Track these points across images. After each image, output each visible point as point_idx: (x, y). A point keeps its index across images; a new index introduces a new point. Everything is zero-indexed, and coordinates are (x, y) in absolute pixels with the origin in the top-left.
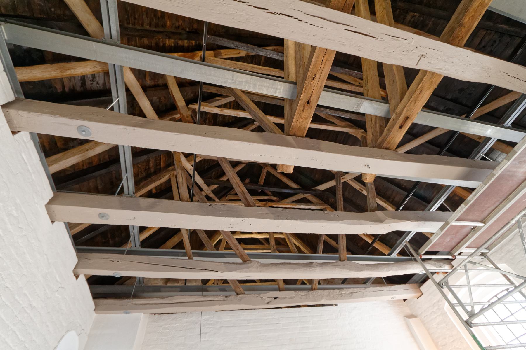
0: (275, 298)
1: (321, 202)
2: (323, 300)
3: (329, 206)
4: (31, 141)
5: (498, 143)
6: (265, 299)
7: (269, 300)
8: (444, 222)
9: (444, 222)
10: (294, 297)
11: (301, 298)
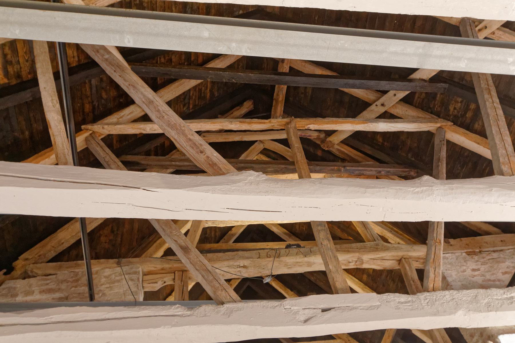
0: (324, 311)
1: (428, 116)
2: (460, 313)
3: (450, 123)
4: (35, 55)
5: (77, 77)
6: (297, 313)
7: (308, 313)
8: (408, 78)
9: (408, 78)
10: (378, 307)
11: (397, 308)
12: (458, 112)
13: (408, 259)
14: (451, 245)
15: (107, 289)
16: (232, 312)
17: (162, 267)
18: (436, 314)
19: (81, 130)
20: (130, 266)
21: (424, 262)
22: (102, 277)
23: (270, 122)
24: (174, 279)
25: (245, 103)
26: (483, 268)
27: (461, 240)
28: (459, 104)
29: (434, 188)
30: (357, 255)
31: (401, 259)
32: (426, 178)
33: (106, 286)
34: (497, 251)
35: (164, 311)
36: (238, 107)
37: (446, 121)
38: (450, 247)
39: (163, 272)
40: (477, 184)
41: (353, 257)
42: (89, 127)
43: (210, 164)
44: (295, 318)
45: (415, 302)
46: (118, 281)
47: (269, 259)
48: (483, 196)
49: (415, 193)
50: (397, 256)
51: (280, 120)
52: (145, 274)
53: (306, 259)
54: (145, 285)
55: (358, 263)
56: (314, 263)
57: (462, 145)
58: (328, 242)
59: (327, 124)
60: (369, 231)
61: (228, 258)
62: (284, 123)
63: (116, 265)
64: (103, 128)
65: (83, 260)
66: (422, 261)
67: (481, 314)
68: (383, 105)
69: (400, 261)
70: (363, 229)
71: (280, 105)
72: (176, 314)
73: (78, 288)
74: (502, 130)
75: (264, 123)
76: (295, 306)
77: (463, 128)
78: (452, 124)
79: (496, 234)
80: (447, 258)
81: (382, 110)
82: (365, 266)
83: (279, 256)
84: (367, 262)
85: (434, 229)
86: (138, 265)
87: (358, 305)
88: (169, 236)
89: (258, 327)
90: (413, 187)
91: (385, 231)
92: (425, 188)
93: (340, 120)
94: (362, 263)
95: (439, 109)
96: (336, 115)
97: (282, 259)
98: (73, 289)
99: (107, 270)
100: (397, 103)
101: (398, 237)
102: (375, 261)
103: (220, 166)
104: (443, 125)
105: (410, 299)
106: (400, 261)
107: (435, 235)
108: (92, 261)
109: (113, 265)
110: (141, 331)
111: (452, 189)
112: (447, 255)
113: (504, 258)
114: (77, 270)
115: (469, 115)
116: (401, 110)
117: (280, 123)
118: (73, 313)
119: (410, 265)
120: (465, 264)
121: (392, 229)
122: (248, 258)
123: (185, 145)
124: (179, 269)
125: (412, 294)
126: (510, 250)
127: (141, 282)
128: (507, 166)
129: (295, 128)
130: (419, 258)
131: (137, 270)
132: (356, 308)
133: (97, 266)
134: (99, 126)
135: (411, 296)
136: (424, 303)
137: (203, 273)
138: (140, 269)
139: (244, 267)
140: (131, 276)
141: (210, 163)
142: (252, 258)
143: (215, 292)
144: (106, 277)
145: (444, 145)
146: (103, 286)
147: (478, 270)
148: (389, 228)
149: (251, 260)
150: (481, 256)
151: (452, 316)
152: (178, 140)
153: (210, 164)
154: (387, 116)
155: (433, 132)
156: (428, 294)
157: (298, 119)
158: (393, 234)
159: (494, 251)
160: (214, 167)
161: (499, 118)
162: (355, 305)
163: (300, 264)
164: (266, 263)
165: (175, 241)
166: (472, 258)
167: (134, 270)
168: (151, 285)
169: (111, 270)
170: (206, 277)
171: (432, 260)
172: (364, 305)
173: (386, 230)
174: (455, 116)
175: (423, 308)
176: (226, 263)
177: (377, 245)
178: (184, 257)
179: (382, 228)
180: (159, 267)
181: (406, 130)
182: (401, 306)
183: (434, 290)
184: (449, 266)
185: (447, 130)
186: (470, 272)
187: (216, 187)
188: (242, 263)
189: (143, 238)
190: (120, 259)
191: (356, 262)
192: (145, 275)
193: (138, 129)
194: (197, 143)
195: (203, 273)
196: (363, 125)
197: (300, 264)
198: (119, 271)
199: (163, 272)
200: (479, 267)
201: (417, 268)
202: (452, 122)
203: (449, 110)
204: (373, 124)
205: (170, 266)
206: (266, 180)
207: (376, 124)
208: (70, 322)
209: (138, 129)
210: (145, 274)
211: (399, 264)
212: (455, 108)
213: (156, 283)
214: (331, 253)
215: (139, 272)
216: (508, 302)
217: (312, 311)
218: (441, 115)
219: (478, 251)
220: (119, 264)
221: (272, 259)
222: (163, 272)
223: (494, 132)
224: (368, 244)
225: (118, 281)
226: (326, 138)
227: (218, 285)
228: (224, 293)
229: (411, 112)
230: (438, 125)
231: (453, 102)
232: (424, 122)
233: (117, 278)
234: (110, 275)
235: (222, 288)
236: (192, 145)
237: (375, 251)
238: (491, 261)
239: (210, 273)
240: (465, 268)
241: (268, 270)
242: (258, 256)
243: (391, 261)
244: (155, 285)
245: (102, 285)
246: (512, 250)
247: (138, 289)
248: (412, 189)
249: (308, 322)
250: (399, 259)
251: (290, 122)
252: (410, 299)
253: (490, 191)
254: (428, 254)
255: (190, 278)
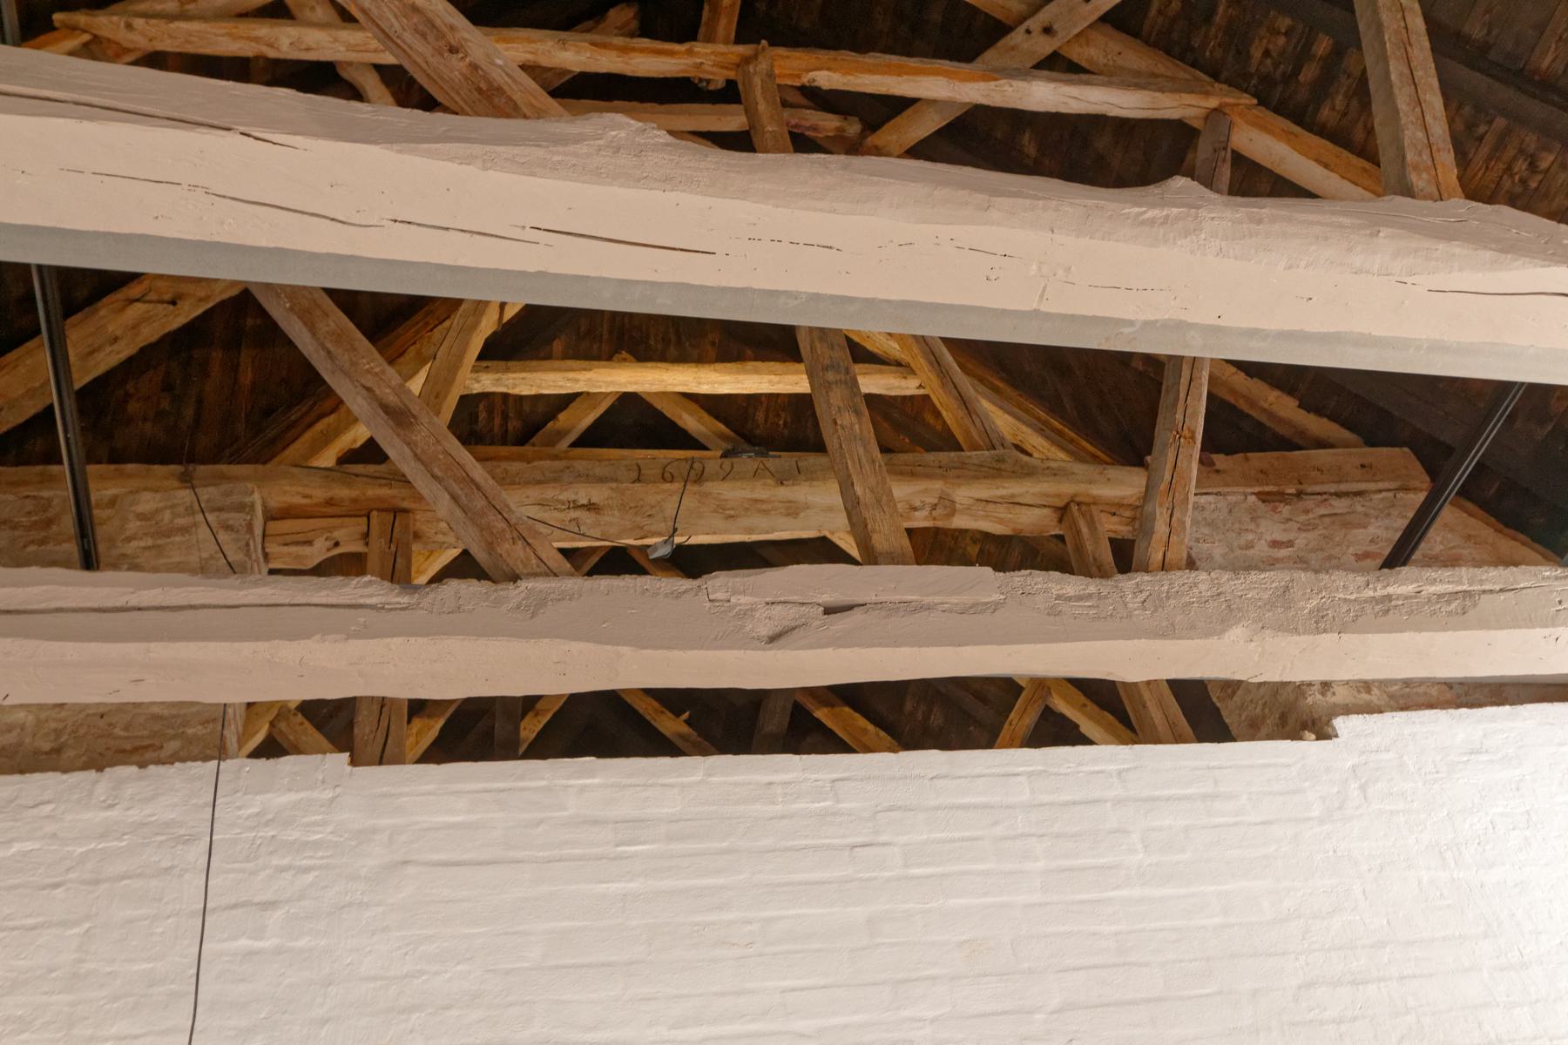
0: (829, 611)
1: (1183, 72)
2: (1237, 633)
7: (782, 616)
10: (996, 607)
11: (1053, 612)
12: (1276, 65)
13: (1088, 505)
14: (1218, 471)
15: (147, 553)
16: (542, 603)
17: (329, 494)
18: (1168, 632)
19: (49, 27)
20: (225, 487)
21: (1134, 519)
22: (131, 516)
23: (690, 52)
24: (366, 535)
25: (612, 13)
26: (1301, 540)
27: (1247, 459)
28: (1282, 40)
29: (1202, 213)
30: (938, 485)
31: (1067, 505)
32: (1180, 182)
33: (142, 544)
34: (1346, 494)
35: (324, 593)
36: (590, 23)
37: (1237, 93)
38: (1214, 476)
39: (330, 510)
40: (1333, 213)
41: (926, 491)
42: (81, 18)
43: (479, 90)
44: (742, 627)
45: (1106, 597)
46: (184, 530)
47: (667, 486)
48: (1349, 250)
49: (1143, 223)
50: (1059, 496)
51: (721, 48)
52: (271, 516)
53: (783, 492)
54: (272, 548)
55: (938, 512)
56: (807, 507)
57: (1277, 171)
58: (854, 419)
59: (871, 72)
60: (977, 421)
61: (539, 477)
62: (734, 59)
63: (176, 484)
64: (129, 26)
65: (60, 462)
66: (1128, 514)
67: (1296, 638)
68: (1048, 30)
69: (1063, 512)
70: (961, 413)
71: (723, 21)
72: (362, 601)
73: (50, 547)
74: (1418, 74)
75: (671, 53)
76: (744, 593)
77: (1288, 116)
78: (1255, 101)
79: (1347, 445)
80: (1203, 509)
81: (1046, 46)
82: (960, 522)
83: (700, 479)
84: (968, 509)
85: (1177, 399)
86: (250, 485)
87: (938, 599)
88: (347, 374)
89: (624, 650)
90: (1140, 206)
91: (1024, 428)
92: (1175, 210)
93: (913, 62)
94: (952, 512)
95: (1219, 54)
96: (905, 48)
97: (709, 486)
98: (32, 548)
99: (147, 496)
100: (1091, 26)
101: (1063, 449)
102: (991, 506)
103: (517, 97)
104: (1227, 105)
105: (1092, 589)
106: (1063, 512)
107: (1179, 416)
108: (92, 469)
109: (166, 483)
110: (246, 648)
111: (1260, 222)
112: (1203, 499)
113: (1366, 515)
114: (45, 494)
115: (1309, 73)
116: (1104, 49)
117: (719, 59)
118: (15, 585)
119: (1092, 524)
120: (1252, 526)
121: (1045, 423)
122: (602, 480)
123: (396, 25)
124: (385, 506)
125: (1102, 577)
126: (1384, 494)
127: (259, 540)
128: (1425, 176)
129: (770, 75)
130: (1120, 505)
131: (247, 500)
132: (929, 608)
133: (105, 485)
134: (115, 18)
135: (1098, 581)
136: (1133, 603)
137: (456, 489)
138: (256, 497)
139: (591, 507)
140: (224, 516)
141: (484, 86)
142: (616, 480)
143: (490, 547)
144: (142, 517)
145: (1224, 160)
146: (134, 544)
147: (1290, 544)
148: (1039, 419)
149: (614, 485)
150: (1301, 505)
151: (1213, 642)
152: (375, 12)
153: (479, 90)
154: (1057, 65)
155: (1196, 124)
156: (1147, 577)
157: (781, 51)
158: (1047, 438)
159: (1338, 495)
160: (496, 100)
161: (1413, 38)
162: (927, 600)
163: (764, 507)
164: (659, 497)
165: (368, 389)
166: (1274, 510)
167: (236, 498)
168: (293, 549)
169: (158, 496)
170: (463, 499)
171: (1163, 486)
172: (954, 599)
173: (1029, 425)
174: (1266, 80)
175: (1130, 616)
176: (534, 493)
177: (1000, 460)
178: (397, 441)
179: (1018, 418)
180: (319, 493)
181: (1114, 112)
182: (1064, 607)
183: (1164, 567)
184: (1206, 531)
185: (1237, 120)
186: (1266, 548)
187: (498, 149)
188: (583, 494)
189: (268, 412)
190: (191, 467)
191: (934, 507)
192: (274, 519)
193: (249, 39)
194: (438, 22)
195: (456, 489)
196: (982, 85)
197: (764, 507)
198: (188, 500)
199: (331, 510)
200: (1291, 536)
201: (1112, 535)
202: (1255, 95)
203: (1249, 57)
204: (1015, 83)
205: (354, 493)
206: (667, 145)
207: (1025, 84)
208: (9, 612)
209: (249, 39)
210: (271, 516)
211: (1060, 521)
212: (1267, 53)
213: (309, 543)
214: (861, 451)
215: (252, 506)
216: (1377, 608)
217: (793, 611)
218: (1225, 75)
219: (1293, 491)
220: (186, 480)
221: (677, 486)
222: (331, 510)
223: (1393, 77)
224: (974, 456)
225: (184, 530)
226: (865, 137)
227: (502, 525)
228: (519, 550)
229: (1136, 58)
230: (1213, 103)
231: (1263, 31)
232: (1172, 91)
233: (180, 521)
234: (157, 511)
235: (515, 534)
236: (421, 28)
237: (994, 477)
238: (1327, 520)
239: (478, 488)
240: (1250, 537)
241: (665, 520)
242: (634, 475)
243: (1037, 511)
244: (306, 550)
245: (129, 539)
246: (1391, 494)
247: (248, 554)
248: (1136, 210)
249: (782, 642)
250: (1060, 504)
251: (755, 56)
252: (1092, 589)
253: (1371, 235)
254: (1147, 494)
255: (417, 536)
